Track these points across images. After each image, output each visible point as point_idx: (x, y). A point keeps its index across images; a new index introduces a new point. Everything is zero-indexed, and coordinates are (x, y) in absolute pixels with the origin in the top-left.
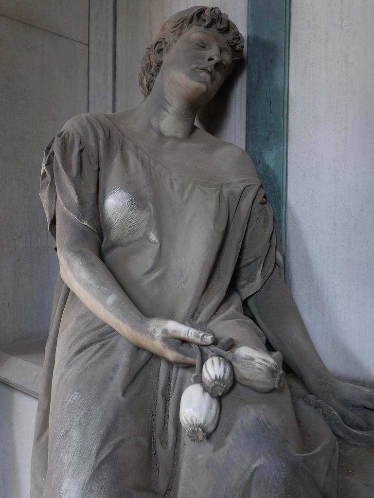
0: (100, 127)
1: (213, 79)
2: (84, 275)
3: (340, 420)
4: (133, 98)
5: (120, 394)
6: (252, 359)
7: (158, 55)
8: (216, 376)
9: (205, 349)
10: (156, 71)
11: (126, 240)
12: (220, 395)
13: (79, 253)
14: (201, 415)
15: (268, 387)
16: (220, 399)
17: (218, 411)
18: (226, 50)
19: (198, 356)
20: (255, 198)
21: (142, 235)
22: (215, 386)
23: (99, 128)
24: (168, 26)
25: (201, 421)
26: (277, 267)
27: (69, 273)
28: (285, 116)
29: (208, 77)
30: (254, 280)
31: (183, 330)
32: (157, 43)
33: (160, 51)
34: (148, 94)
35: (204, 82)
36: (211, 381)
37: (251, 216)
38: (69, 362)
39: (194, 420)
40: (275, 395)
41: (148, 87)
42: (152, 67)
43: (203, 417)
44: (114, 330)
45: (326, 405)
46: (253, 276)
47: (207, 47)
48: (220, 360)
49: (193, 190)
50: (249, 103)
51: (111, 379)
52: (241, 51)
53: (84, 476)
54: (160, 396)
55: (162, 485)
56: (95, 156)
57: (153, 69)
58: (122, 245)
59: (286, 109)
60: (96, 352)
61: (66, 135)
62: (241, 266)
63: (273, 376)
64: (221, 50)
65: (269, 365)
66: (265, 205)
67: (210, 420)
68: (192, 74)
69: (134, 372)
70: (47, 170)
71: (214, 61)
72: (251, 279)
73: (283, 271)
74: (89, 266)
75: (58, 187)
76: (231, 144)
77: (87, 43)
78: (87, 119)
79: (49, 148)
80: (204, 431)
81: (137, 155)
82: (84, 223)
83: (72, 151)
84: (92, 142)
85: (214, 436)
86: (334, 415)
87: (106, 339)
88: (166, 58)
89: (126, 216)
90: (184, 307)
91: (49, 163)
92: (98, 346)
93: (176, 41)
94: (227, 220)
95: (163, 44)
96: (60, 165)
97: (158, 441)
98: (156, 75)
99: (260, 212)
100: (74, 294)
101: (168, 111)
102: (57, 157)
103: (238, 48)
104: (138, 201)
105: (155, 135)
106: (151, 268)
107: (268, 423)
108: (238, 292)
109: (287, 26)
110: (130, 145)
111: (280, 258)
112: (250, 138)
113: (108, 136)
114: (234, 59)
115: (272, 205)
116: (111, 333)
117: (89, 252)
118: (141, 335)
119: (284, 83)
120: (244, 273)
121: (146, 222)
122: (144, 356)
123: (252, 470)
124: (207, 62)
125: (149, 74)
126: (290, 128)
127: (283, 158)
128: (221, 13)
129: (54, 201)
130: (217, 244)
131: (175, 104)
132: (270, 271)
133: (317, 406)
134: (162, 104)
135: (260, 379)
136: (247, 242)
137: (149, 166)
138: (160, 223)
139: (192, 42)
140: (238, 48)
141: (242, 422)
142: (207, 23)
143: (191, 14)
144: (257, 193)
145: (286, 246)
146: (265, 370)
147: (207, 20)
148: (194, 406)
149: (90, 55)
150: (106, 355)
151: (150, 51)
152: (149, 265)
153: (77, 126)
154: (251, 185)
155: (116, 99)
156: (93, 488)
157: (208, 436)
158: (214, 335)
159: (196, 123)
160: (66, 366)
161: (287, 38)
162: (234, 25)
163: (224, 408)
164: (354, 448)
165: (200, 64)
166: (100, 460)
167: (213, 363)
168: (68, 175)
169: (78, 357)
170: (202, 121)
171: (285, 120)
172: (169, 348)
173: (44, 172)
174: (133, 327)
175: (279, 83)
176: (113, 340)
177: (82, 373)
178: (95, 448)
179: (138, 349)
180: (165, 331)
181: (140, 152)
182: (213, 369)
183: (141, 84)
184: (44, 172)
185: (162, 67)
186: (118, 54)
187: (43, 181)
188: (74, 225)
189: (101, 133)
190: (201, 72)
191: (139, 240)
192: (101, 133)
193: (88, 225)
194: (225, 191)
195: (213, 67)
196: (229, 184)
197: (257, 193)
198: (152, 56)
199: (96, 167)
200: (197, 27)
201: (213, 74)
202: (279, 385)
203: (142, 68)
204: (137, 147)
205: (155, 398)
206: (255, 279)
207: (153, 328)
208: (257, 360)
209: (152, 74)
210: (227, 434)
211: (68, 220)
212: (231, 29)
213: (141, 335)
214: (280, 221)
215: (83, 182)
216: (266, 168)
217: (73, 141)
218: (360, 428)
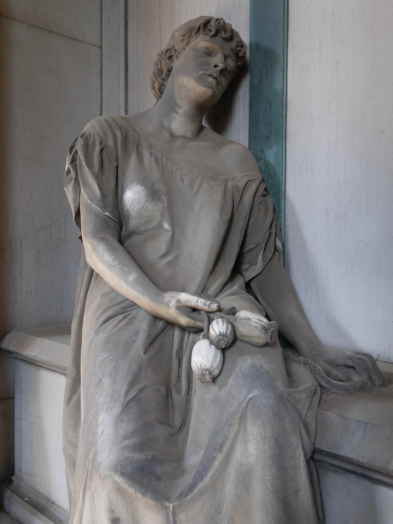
0: (118, 128)
1: (218, 84)
2: (108, 257)
3: (323, 374)
4: (145, 100)
5: (142, 353)
6: (250, 319)
7: (168, 61)
8: (220, 332)
9: (212, 315)
10: (166, 76)
11: (142, 229)
12: (223, 347)
13: (102, 239)
14: (208, 362)
15: (262, 341)
16: (223, 351)
17: (222, 359)
18: (230, 56)
19: (206, 320)
20: (257, 191)
21: (156, 224)
22: (219, 340)
23: (117, 130)
24: (177, 35)
25: (208, 366)
26: (277, 253)
27: (94, 257)
28: (284, 117)
29: (214, 82)
30: (256, 264)
31: (193, 300)
32: (167, 51)
33: (170, 57)
34: (160, 97)
35: (210, 87)
36: (216, 336)
37: (253, 207)
38: (98, 329)
39: (203, 365)
40: (268, 349)
41: (159, 91)
42: (163, 72)
43: (210, 363)
44: (135, 304)
45: (313, 362)
46: (254, 261)
47: (213, 54)
48: (223, 321)
49: (201, 183)
50: (252, 105)
51: (134, 342)
52: (244, 57)
53: (116, 410)
54: (174, 356)
55: (177, 421)
56: (114, 154)
57: (163, 75)
58: (139, 233)
59: (284, 111)
60: (120, 322)
61: (88, 136)
62: (244, 252)
63: (266, 332)
64: (226, 57)
65: (262, 323)
66: (266, 197)
67: (215, 365)
68: (200, 80)
69: (153, 337)
70: (72, 166)
71: (218, 68)
72: (253, 263)
73: (282, 256)
74: (112, 250)
75: (83, 182)
76: (236, 142)
77: (99, 45)
78: (105, 120)
79: (72, 148)
80: (210, 373)
81: (151, 153)
82: (107, 214)
83: (93, 151)
84: (111, 142)
85: (219, 379)
86: (319, 370)
87: (128, 312)
88: (176, 64)
89: (142, 207)
90: (196, 282)
91: (73, 161)
92: (121, 316)
93: (185, 49)
94: (102, 75)
95: (173, 51)
96: (84, 163)
97: (173, 390)
98: (167, 80)
99: (261, 203)
100: (97, 275)
101: (178, 113)
102: (81, 155)
103: (241, 54)
104: (153, 194)
105: (167, 135)
106: (165, 252)
107: (261, 367)
108: (242, 274)
109: (286, 35)
110: (144, 144)
111: (279, 244)
112: (252, 137)
113: (125, 137)
114: (237, 64)
115: (272, 198)
116: (131, 307)
117: (112, 239)
118: (158, 305)
119: (283, 86)
120: (247, 258)
121: (160, 213)
122: (160, 324)
123: (247, 400)
124: (213, 68)
125: (161, 78)
126: (288, 127)
127: (282, 155)
128: (225, 23)
129: (78, 195)
130: (223, 230)
131: (184, 107)
132: (270, 256)
133: (305, 364)
134: (172, 107)
135: (256, 335)
136: (249, 231)
137: (162, 163)
138: (172, 213)
139: (199, 50)
140: (241, 54)
141: (241, 367)
142: (213, 32)
143: (198, 24)
144: (259, 186)
145: (285, 234)
146: (259, 327)
147: (212, 30)
148: (203, 355)
149: (103, 57)
150: (129, 324)
151: (161, 57)
152: (164, 250)
153: (97, 128)
154: (253, 179)
155: (129, 100)
156: (124, 419)
157: (214, 379)
158: (219, 305)
159: (204, 123)
160: (95, 333)
161: (286, 45)
162: (237, 34)
163: (226, 359)
164: (334, 395)
165: (207, 70)
166: (128, 399)
167: (218, 323)
168: (91, 171)
169: (104, 326)
170: (209, 121)
171: (284, 120)
172: (182, 315)
173: (69, 169)
174: (151, 299)
175: (278, 86)
176: (134, 313)
177: (109, 337)
178: (123, 391)
179: (156, 318)
180: (179, 301)
181: (154, 151)
182: (218, 327)
183: (153, 88)
184: (69, 169)
185: (172, 72)
186: (130, 57)
187: (67, 177)
188: (97, 216)
189: (118, 134)
190: (208, 78)
191: (154, 229)
192: (118, 134)
193: (109, 215)
194: (230, 185)
195: (218, 73)
196: (233, 179)
197: (259, 186)
198: (163, 62)
199: (115, 165)
200: (203, 36)
201: (218, 79)
202: (271, 339)
203: (154, 72)
204: (151, 147)
205: (171, 358)
206: (256, 264)
207: (169, 299)
208: (253, 320)
209: (163, 79)
210: (229, 377)
211: (90, 211)
212: (234, 37)
213: (158, 305)
214: (280, 212)
215: (104, 178)
216: (267, 164)
217: (94, 141)
218: (340, 381)
